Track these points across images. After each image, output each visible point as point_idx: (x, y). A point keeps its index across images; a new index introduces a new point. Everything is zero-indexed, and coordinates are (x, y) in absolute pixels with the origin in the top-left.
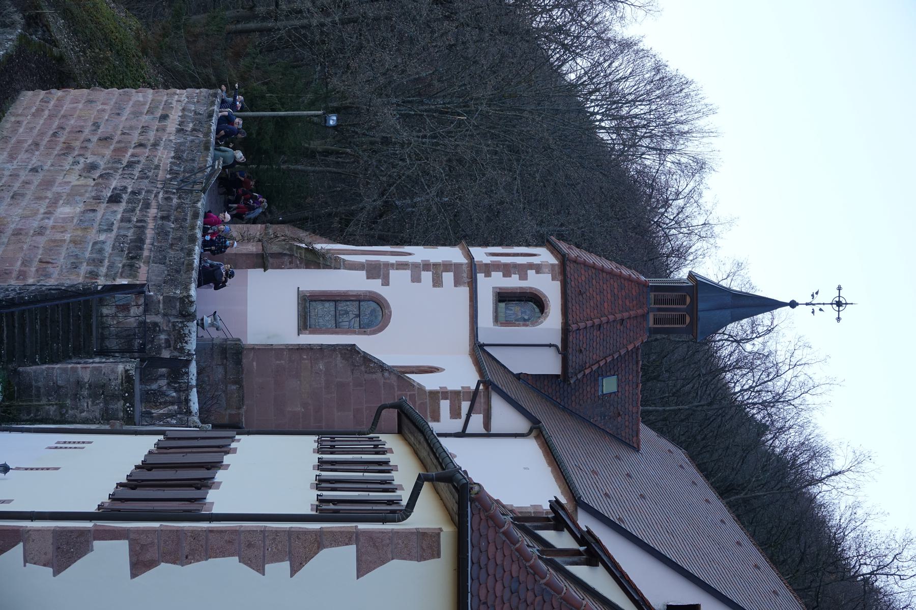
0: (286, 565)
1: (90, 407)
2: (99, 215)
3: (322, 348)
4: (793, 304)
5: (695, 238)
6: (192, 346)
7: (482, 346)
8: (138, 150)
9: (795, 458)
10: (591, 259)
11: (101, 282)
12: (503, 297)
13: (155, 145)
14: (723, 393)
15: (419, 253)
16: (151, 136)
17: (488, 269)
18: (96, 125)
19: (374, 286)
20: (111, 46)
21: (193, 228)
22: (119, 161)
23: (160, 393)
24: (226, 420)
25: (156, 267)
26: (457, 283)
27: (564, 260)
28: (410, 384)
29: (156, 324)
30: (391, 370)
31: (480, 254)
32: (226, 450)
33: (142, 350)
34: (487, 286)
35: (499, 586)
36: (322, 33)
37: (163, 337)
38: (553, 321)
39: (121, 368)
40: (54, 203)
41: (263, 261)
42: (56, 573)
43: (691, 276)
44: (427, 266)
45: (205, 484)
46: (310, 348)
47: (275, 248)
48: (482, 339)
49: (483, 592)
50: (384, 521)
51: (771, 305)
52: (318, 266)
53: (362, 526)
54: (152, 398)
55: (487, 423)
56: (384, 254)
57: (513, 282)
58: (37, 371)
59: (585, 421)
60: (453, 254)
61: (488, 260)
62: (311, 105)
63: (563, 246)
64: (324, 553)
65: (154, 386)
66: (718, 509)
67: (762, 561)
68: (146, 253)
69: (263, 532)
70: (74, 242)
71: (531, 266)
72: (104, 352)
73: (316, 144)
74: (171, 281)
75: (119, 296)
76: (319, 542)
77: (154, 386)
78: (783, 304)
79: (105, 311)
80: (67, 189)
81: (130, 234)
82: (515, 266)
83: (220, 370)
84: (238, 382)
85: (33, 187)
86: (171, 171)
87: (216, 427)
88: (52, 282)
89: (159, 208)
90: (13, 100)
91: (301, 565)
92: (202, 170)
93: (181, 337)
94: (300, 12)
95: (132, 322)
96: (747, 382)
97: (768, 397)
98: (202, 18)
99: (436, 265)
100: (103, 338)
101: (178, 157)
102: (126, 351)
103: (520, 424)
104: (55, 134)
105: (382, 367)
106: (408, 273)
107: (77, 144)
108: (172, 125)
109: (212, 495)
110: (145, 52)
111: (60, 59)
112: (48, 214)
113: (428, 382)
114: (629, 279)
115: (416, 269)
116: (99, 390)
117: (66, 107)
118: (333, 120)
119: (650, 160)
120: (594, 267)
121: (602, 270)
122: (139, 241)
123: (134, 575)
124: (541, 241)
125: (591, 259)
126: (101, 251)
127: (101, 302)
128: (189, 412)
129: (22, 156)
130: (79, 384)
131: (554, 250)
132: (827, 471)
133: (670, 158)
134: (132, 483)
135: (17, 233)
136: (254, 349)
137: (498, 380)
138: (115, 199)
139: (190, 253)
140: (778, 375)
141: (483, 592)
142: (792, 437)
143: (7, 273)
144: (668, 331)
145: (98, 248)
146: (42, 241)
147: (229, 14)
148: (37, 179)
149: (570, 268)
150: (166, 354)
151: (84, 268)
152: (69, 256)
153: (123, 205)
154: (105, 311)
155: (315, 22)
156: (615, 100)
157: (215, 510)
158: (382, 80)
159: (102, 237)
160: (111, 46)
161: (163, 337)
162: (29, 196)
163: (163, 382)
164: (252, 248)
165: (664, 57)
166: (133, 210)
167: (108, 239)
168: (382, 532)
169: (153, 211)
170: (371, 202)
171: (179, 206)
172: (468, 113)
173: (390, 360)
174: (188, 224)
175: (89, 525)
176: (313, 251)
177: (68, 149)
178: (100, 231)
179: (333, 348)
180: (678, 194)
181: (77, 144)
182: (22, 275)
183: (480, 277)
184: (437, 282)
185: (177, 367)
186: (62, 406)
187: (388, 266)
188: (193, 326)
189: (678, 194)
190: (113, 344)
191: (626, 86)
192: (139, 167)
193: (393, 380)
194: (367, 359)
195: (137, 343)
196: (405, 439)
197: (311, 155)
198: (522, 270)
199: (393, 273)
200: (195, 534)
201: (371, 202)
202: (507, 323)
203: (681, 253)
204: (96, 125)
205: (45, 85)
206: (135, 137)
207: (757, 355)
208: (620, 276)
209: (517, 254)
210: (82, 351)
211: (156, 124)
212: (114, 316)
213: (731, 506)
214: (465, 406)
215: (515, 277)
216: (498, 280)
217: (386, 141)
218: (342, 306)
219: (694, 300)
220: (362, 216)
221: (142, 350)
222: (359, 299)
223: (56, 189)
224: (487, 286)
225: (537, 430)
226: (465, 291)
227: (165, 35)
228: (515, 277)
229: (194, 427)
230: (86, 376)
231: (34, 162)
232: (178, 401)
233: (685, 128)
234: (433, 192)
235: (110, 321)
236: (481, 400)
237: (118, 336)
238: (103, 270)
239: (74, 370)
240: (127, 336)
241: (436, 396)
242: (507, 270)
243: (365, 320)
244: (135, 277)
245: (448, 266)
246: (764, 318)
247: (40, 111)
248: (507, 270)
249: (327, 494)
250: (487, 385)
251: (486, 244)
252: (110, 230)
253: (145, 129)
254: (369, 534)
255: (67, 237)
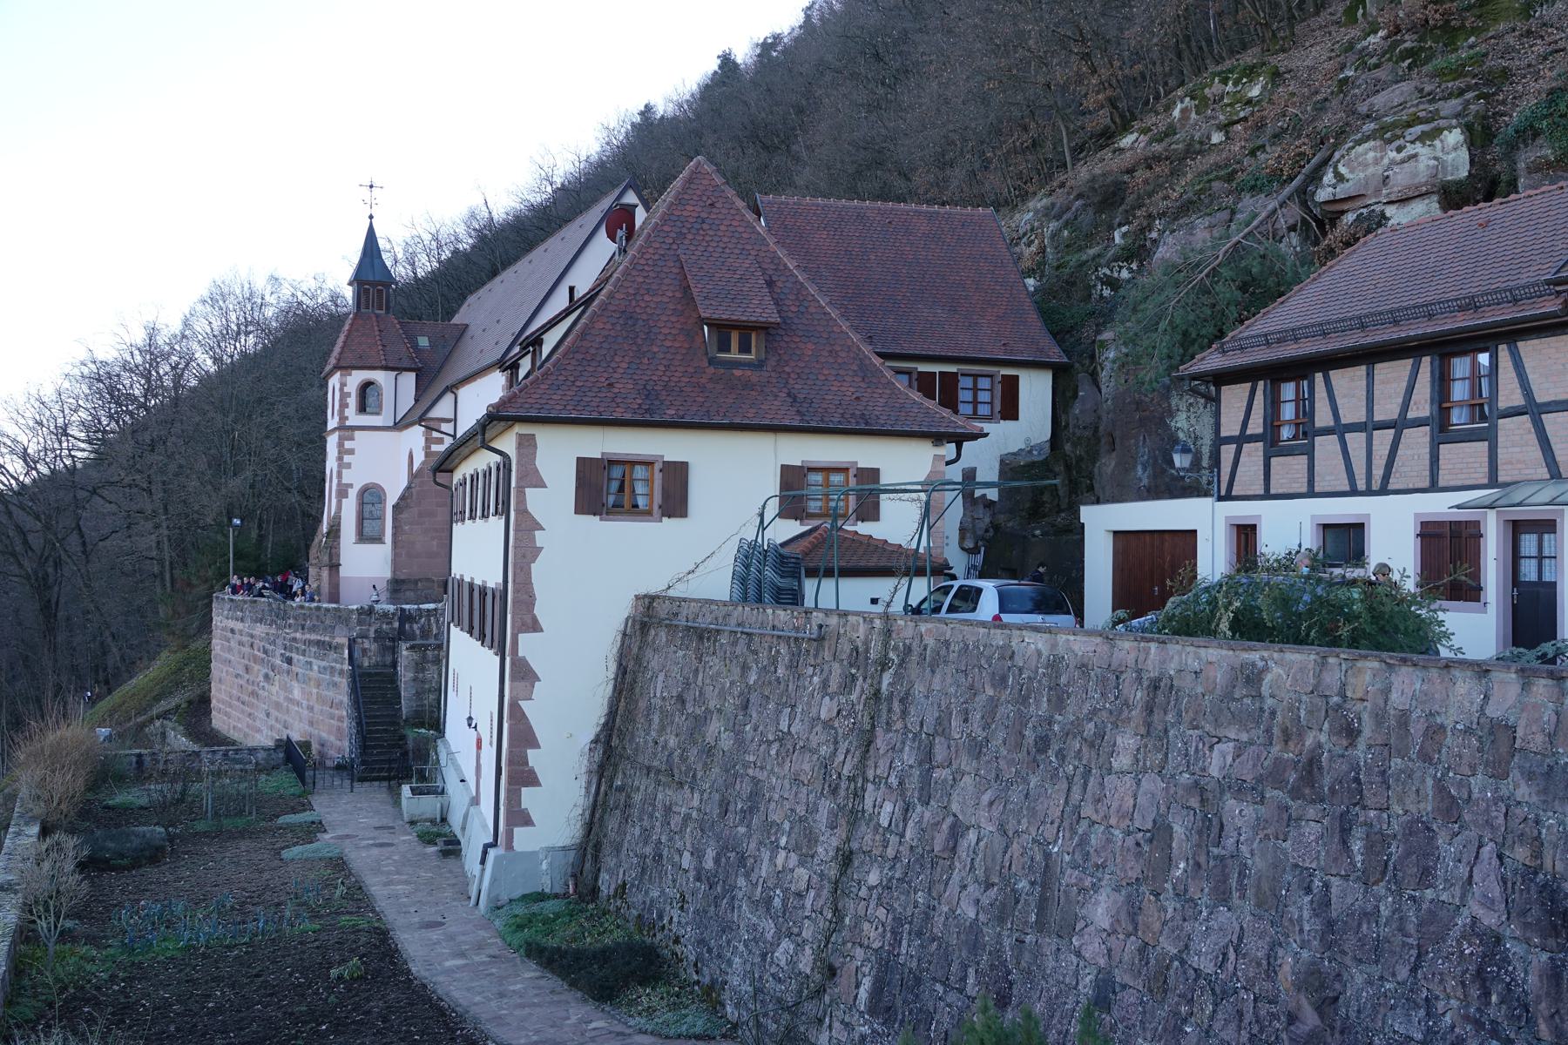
0: (537, 533)
1: (431, 672)
2: (300, 671)
3: (394, 527)
4: (371, 217)
5: (324, 286)
6: (391, 608)
7: (395, 424)
8: (256, 647)
9: (475, 230)
10: (337, 350)
11: (346, 667)
12: (362, 408)
13: (252, 636)
14: (434, 276)
15: (331, 463)
16: (245, 639)
17: (343, 418)
18: (237, 676)
19: (353, 494)
20: (180, 669)
21: (310, 609)
22: (263, 659)
23: (422, 629)
24: (442, 590)
25: (337, 631)
26: (352, 439)
27: (337, 368)
28: (420, 470)
29: (376, 631)
30: (410, 483)
31: (332, 423)
32: (461, 582)
33: (393, 640)
34: (354, 418)
35: (554, 397)
36: (174, 528)
37: (384, 626)
38: (379, 376)
39: (405, 653)
40: (291, 701)
41: (334, 567)
42: (539, 680)
43: (350, 284)
44: (340, 459)
45: (483, 591)
46: (394, 535)
47: (326, 559)
48: (391, 424)
49: (558, 407)
50: (510, 470)
51: (371, 236)
52: (338, 530)
53: (513, 484)
54: (425, 633)
55: (448, 421)
56: (331, 487)
57: (352, 401)
58: (406, 706)
59: (447, 358)
60: (332, 442)
61: (337, 418)
62: (227, 537)
63: (328, 368)
64: (530, 509)
65: (418, 632)
66: (507, 275)
67: (541, 248)
68: (327, 639)
69: (515, 547)
70: (318, 686)
71: (341, 390)
72: (394, 664)
73: (254, 534)
74: (347, 621)
75: (356, 655)
76: (523, 512)
77: (418, 632)
78: (371, 224)
79: (366, 664)
80: (282, 693)
81: (313, 650)
82: (341, 400)
83: (408, 593)
84: (416, 582)
85: (280, 716)
86: (271, 625)
87: (446, 593)
88: (346, 699)
89: (296, 631)
90: (218, 732)
91: (538, 524)
92: (270, 604)
93: (385, 615)
94: (158, 543)
95: (374, 647)
96: (423, 258)
97: (434, 244)
98: (162, 610)
99: (339, 452)
100: (385, 666)
101: (261, 621)
102: (394, 650)
103: (448, 399)
104: (243, 703)
105: (408, 488)
106: (344, 471)
107: (250, 688)
108: (238, 626)
109: (491, 584)
110: (186, 647)
111: (190, 702)
112: (298, 704)
113: (419, 458)
114: (352, 325)
115: (342, 465)
116: (419, 667)
117: (223, 696)
118: (237, 521)
119: (269, 312)
120: (343, 348)
121: (345, 342)
122: (319, 643)
123: (542, 630)
124: (324, 385)
125: (337, 350)
126: (325, 668)
127: (360, 667)
128: (435, 610)
129: (258, 724)
130: (415, 679)
131: (331, 374)
132: (484, 208)
133: (267, 298)
134: (482, 638)
135: (311, 723)
136: (394, 571)
137: (419, 412)
138: (289, 661)
139: (327, 610)
140: (419, 237)
141: (558, 407)
142: (461, 230)
143: (339, 729)
144: (388, 302)
145: (322, 670)
146: (317, 707)
147: (159, 590)
148: (274, 713)
149: (343, 364)
150: (396, 625)
151: (337, 679)
152: (328, 689)
153: (294, 655)
154: (366, 664)
155: (166, 532)
156: (225, 335)
157: (500, 580)
158: (209, 487)
159: (315, 668)
160: (180, 669)
161: (384, 626)
162: (286, 717)
163: (415, 626)
164: (325, 573)
165: (196, 297)
166: (297, 648)
167: (316, 664)
168: (518, 471)
169: (298, 635)
170: (294, 498)
171: (295, 619)
172: (233, 430)
173: (403, 483)
174: (308, 612)
175: (508, 660)
176: (328, 533)
177: (253, 694)
178: (311, 669)
179: (394, 519)
180: (293, 295)
181: (250, 688)
182: (340, 719)
183: (348, 423)
184: (351, 452)
185: (405, 617)
186: (430, 691)
187: (339, 484)
188: (377, 607)
189: (293, 295)
190: (389, 659)
191: (216, 324)
192: (267, 646)
193: (417, 481)
194: (402, 498)
195: (388, 643)
196: (457, 467)
197: (261, 538)
198: (344, 396)
199: (344, 481)
200: (516, 591)
201: (294, 498)
202: (380, 406)
203: (335, 298)
204: (237, 676)
205: (208, 712)
206: (247, 650)
207: (405, 251)
208: (349, 331)
209: (333, 399)
210: (392, 679)
211: (237, 636)
212: (370, 658)
213: (504, 268)
214: (435, 434)
215: (349, 400)
216: (351, 411)
217: (252, 486)
218: (366, 515)
219: (368, 283)
220: (304, 503)
221: (393, 640)
222: (362, 503)
223: (281, 700)
224: (354, 418)
225: (452, 388)
226: (357, 434)
227: (174, 634)
228: (349, 400)
229: (446, 606)
230: (410, 675)
231: (262, 716)
232: (428, 616)
233: (247, 286)
234: (288, 456)
235: (373, 661)
236: (431, 424)
237: (383, 656)
238: (338, 666)
239: (405, 683)
240: (384, 650)
241: (428, 454)
242: (344, 405)
243: (376, 500)
244: (343, 645)
245: (340, 445)
246: (382, 244)
247: (226, 714)
248: (344, 405)
249: (492, 509)
250: (421, 420)
251: (325, 423)
252: (311, 663)
253: (241, 643)
254: (519, 479)
255: (315, 691)
